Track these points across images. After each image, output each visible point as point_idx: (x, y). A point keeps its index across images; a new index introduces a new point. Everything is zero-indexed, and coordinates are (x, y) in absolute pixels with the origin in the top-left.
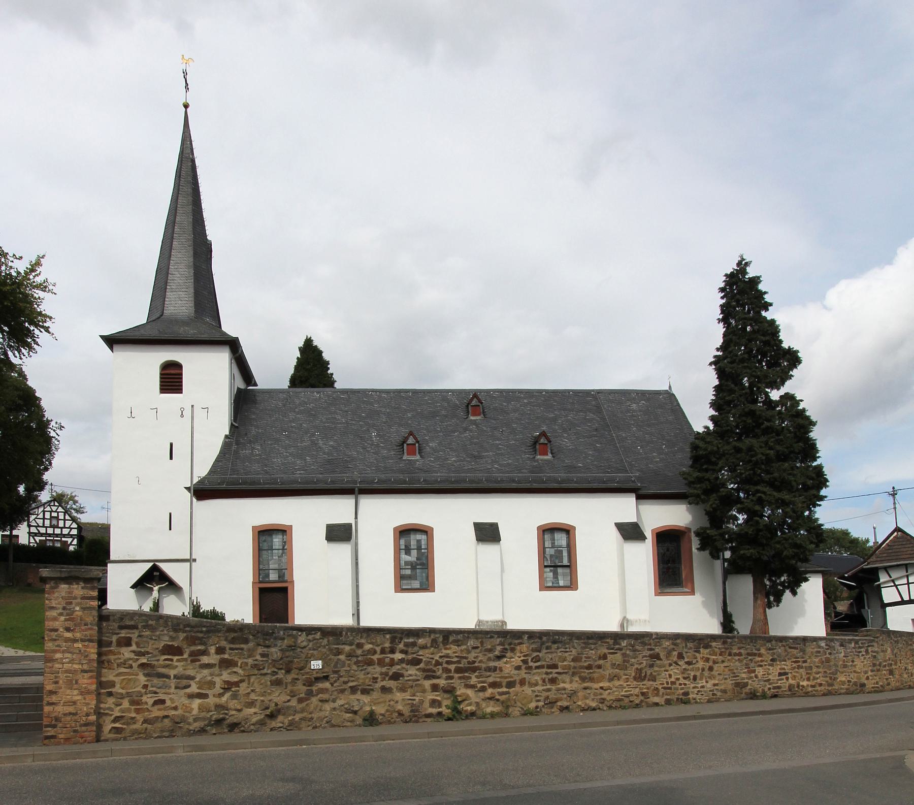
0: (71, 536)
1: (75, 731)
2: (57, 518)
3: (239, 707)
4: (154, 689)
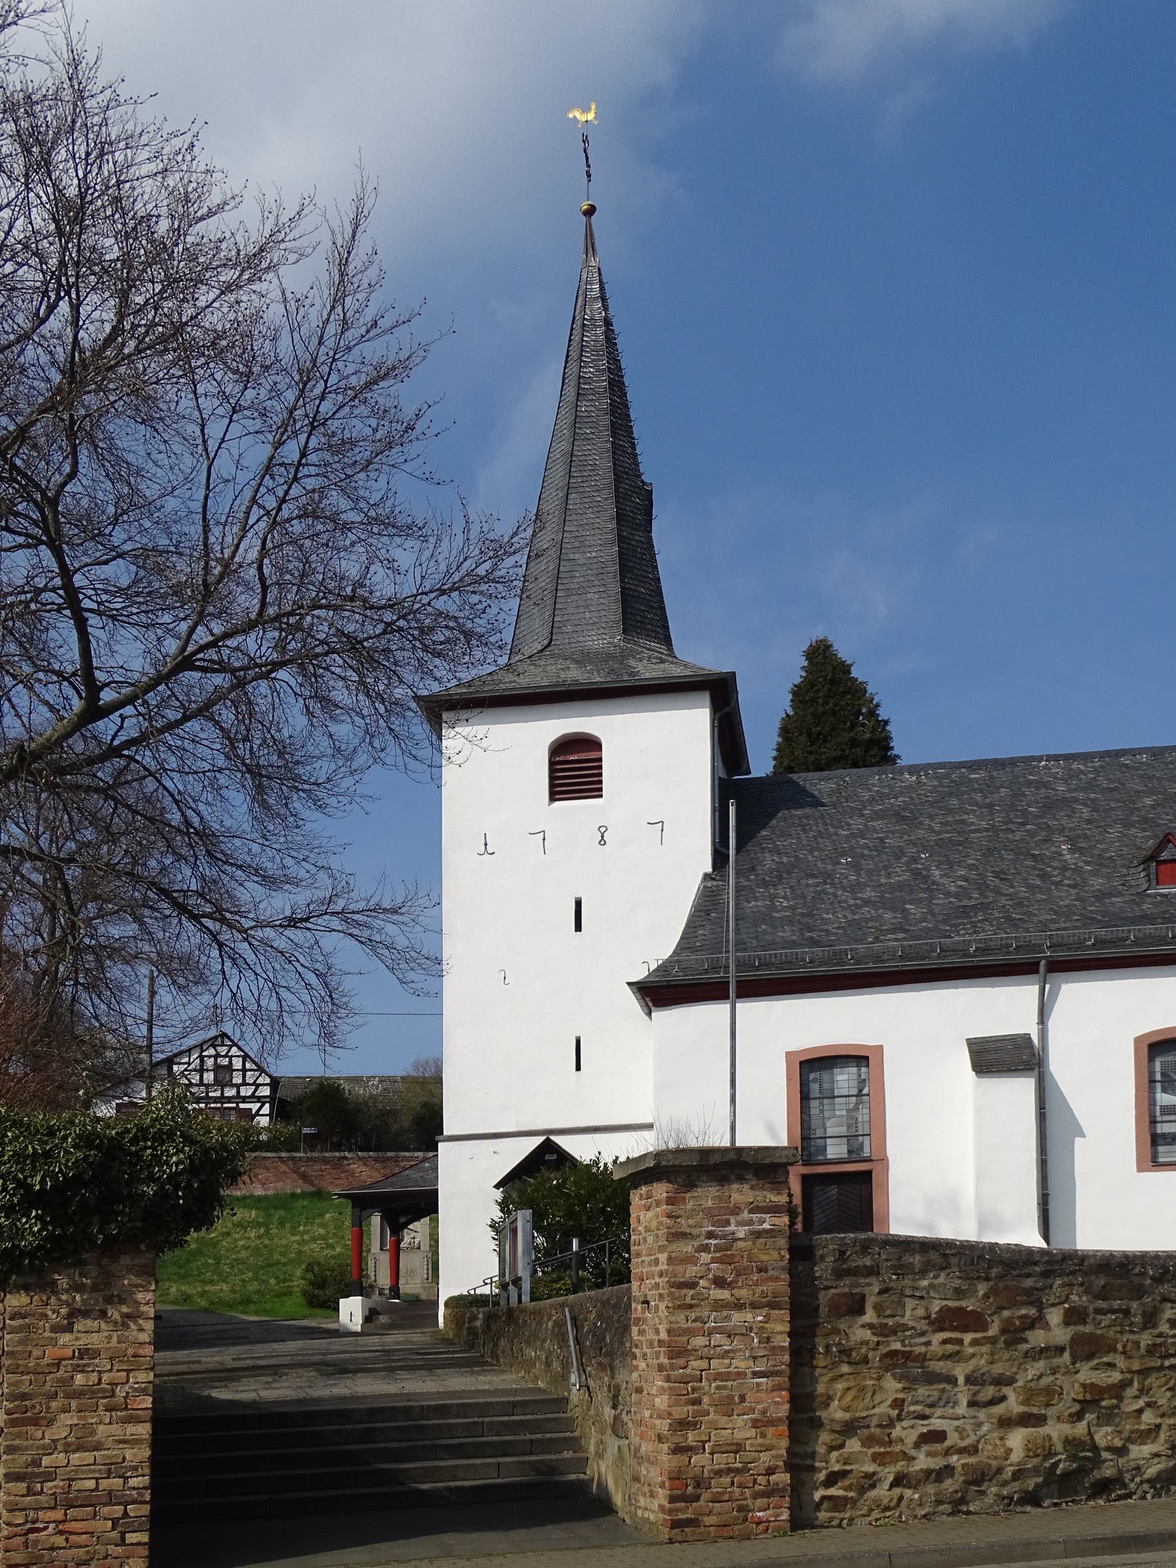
0: (259, 1099)
1: (741, 1509)
2: (229, 1068)
3: (1118, 1443)
4: (918, 1408)
